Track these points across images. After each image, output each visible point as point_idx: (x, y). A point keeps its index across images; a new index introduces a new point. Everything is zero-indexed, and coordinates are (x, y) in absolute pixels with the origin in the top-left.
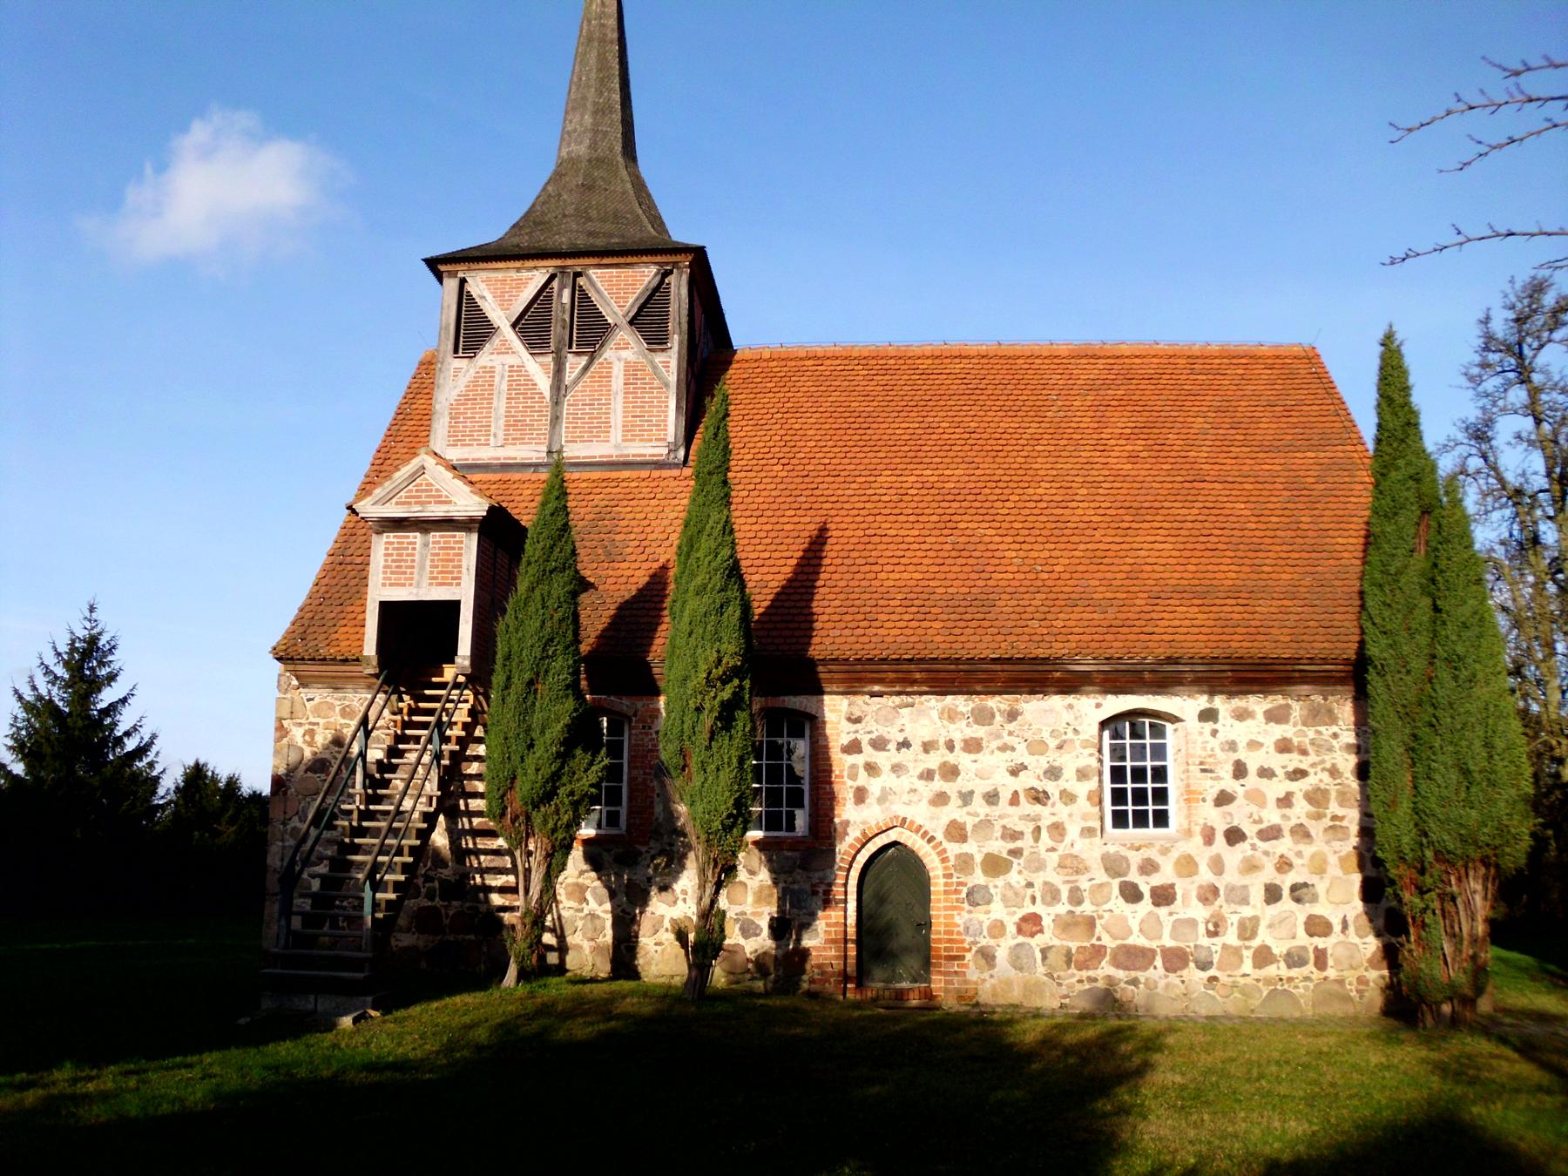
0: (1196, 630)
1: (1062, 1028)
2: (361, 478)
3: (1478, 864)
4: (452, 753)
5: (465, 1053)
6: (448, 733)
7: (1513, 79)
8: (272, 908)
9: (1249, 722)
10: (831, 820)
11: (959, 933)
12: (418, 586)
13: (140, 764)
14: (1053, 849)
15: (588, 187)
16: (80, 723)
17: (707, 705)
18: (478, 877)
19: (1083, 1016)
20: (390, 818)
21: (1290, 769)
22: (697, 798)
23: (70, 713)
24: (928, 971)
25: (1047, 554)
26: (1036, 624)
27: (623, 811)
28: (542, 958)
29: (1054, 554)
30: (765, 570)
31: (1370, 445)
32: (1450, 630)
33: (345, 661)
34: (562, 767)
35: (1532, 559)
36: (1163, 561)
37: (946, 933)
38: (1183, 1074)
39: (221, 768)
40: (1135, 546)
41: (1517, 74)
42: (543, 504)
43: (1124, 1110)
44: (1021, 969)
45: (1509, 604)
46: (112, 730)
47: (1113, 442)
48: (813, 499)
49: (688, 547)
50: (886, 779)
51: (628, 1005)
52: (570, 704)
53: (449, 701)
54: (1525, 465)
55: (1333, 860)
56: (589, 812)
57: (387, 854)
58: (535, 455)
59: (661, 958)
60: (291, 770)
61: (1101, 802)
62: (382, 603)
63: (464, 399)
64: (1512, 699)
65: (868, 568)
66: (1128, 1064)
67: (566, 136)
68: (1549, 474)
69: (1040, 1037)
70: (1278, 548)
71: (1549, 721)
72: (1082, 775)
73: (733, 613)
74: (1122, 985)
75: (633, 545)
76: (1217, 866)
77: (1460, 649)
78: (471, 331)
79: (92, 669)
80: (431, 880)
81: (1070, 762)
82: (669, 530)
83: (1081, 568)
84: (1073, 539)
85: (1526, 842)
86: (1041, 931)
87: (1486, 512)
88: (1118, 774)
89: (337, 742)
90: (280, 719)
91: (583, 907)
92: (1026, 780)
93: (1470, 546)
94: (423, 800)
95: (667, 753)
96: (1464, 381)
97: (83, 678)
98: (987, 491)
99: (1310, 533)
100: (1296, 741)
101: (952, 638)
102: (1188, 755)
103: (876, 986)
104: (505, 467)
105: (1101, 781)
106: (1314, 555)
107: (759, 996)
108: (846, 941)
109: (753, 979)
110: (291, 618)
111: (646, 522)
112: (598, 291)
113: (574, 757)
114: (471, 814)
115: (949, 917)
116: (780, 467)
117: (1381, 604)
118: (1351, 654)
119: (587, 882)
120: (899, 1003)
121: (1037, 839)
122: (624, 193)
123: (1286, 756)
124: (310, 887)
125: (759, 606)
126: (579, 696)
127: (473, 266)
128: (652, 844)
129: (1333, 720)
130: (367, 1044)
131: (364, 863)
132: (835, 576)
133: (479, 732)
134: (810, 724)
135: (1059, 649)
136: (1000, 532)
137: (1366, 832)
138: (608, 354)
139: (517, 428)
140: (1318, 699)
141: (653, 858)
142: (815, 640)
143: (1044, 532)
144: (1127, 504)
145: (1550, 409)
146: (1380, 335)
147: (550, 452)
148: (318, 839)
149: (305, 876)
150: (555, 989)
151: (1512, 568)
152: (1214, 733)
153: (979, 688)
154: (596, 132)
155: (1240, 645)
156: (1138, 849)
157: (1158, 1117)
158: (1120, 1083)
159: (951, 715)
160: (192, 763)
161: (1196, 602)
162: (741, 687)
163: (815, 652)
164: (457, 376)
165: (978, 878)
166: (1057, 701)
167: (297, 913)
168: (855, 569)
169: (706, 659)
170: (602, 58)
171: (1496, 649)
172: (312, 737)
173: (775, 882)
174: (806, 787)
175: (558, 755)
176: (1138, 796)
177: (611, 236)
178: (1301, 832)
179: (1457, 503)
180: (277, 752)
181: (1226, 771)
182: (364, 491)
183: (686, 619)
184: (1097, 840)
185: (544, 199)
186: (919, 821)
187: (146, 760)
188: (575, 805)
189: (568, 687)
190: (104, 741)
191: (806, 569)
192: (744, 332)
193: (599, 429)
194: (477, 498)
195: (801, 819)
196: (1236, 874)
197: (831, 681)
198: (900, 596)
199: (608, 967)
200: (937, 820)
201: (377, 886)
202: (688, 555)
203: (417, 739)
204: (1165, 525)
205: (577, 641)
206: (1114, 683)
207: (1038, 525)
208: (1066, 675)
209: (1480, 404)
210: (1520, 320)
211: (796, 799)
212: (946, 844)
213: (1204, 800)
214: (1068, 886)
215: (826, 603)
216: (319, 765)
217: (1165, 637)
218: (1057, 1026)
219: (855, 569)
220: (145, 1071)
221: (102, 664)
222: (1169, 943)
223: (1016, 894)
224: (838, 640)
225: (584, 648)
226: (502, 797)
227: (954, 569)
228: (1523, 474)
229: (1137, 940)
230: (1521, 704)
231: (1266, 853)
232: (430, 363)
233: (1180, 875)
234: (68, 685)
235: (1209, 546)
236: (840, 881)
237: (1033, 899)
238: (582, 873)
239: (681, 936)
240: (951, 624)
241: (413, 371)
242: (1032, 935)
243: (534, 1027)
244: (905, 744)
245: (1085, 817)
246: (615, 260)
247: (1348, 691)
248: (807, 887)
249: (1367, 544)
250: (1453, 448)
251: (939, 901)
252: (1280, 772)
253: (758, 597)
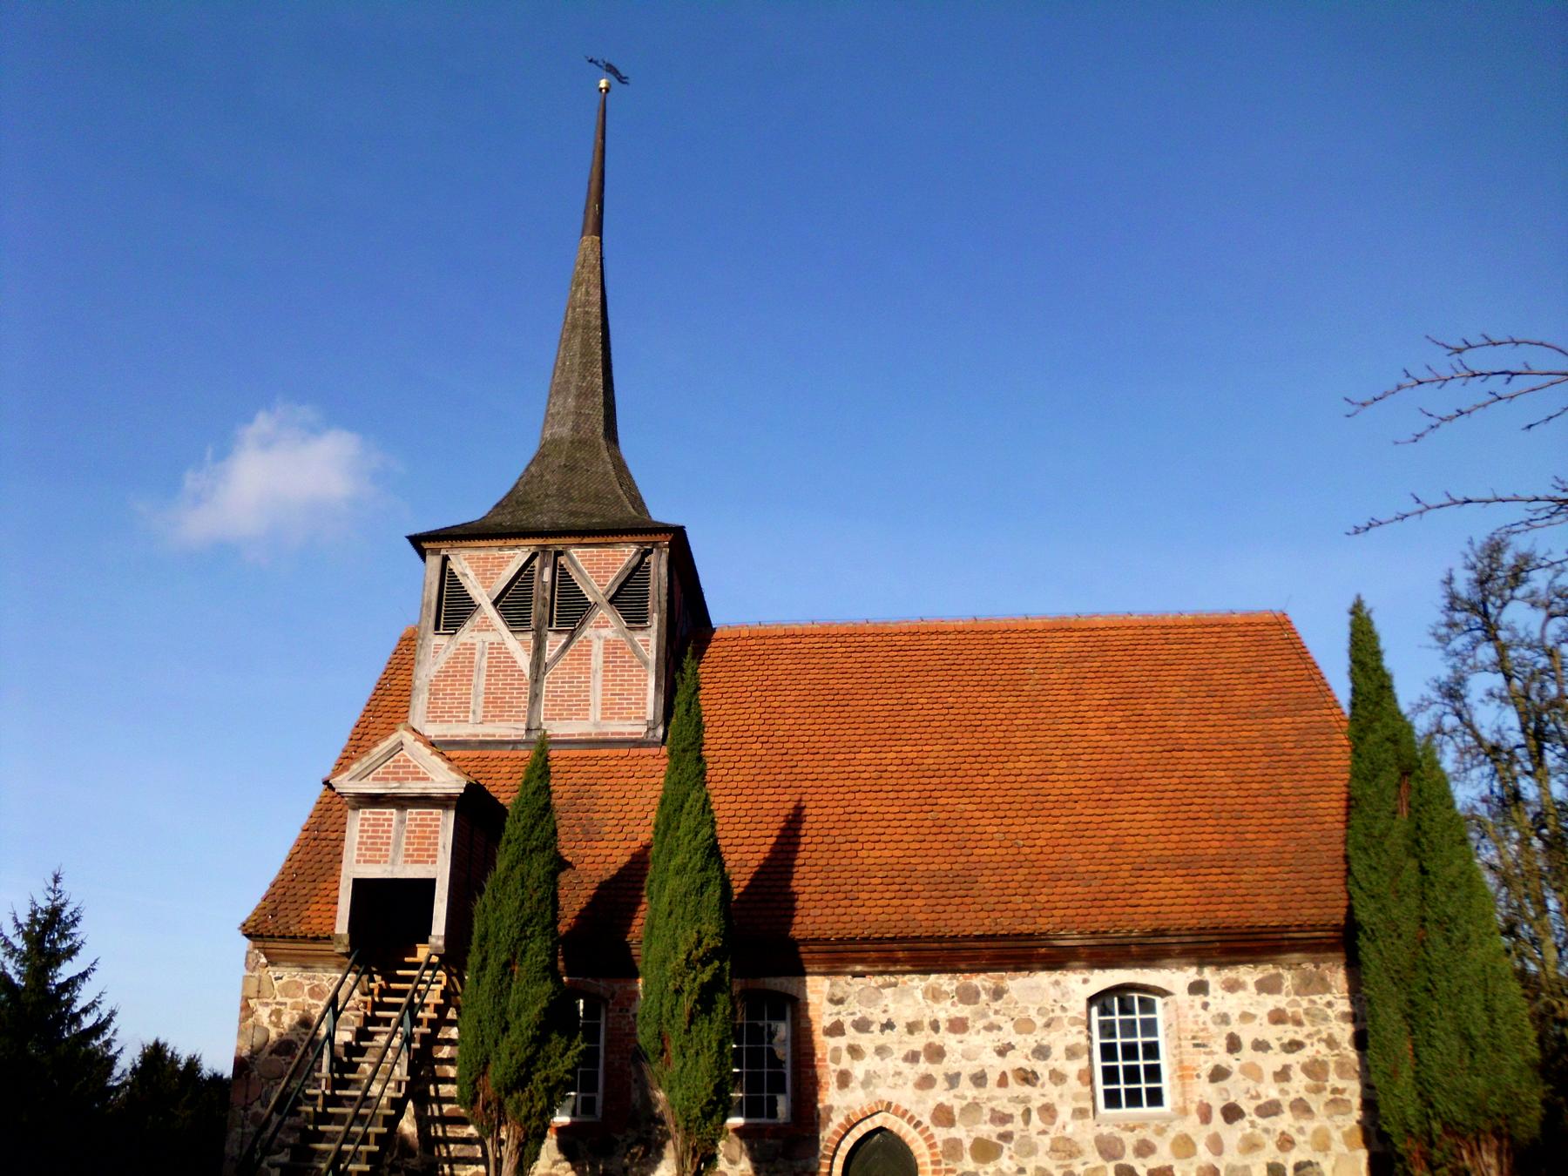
0: (1182, 901)
2: (339, 753)
3: (1490, 1136)
4: (423, 1035)
6: (420, 1014)
7: (1457, 356)
9: (1241, 993)
10: (814, 1106)
12: (393, 863)
13: (96, 1043)
14: (1044, 1132)
15: (571, 467)
17: (687, 988)
20: (356, 1104)
21: (1286, 1040)
22: (676, 1084)
26: (1019, 899)
27: (599, 1098)
30: (744, 849)
31: (1346, 709)
32: (1438, 892)
33: (316, 939)
34: (537, 1052)
35: (1515, 815)
39: (182, 1047)
40: (1117, 817)
41: (1459, 351)
42: (526, 783)
45: (1496, 862)
47: (1091, 714)
48: (792, 777)
49: (666, 826)
50: (870, 1062)
52: (548, 986)
54: (1499, 721)
55: (1337, 1136)
56: (564, 1098)
57: (351, 1142)
58: (513, 732)
60: (255, 1052)
61: (1092, 1081)
62: (355, 881)
63: (445, 674)
64: (1507, 960)
65: (848, 846)
67: (549, 418)
68: (1524, 730)
70: (1260, 815)
71: (1548, 981)
72: (1072, 1053)
73: (713, 893)
75: (611, 828)
76: (1216, 1145)
77: (1450, 910)
78: (453, 608)
79: (53, 942)
81: (1060, 1040)
82: (648, 808)
84: (1054, 812)
85: (1537, 1112)
87: (1466, 770)
88: (1108, 1052)
89: (305, 1022)
90: (246, 999)
92: (1016, 1060)
93: (1452, 805)
94: (392, 1085)
95: (645, 1036)
96: (1432, 641)
99: (1291, 799)
100: (1289, 1011)
101: (933, 916)
102: (1179, 1030)
104: (483, 744)
105: (1091, 1059)
106: (1296, 820)
110: (262, 893)
111: (624, 801)
112: (579, 570)
113: (550, 1041)
114: (441, 1100)
116: (759, 745)
117: (1363, 865)
118: (1340, 919)
121: (1027, 1121)
123: (1280, 1027)
125: (739, 885)
126: (556, 978)
127: (458, 544)
129: (1326, 988)
131: (327, 1152)
132: (815, 855)
133: (451, 1014)
134: (794, 1007)
135: (1043, 924)
136: (982, 807)
137: (1369, 1105)
138: (588, 632)
139: (496, 705)
140: (1310, 967)
141: (630, 1147)
142: (797, 920)
144: (1107, 776)
145: (1519, 665)
146: (1349, 605)
147: (528, 730)
148: (280, 1124)
149: (264, 1165)
151: (1495, 825)
152: (1205, 1006)
153: (963, 966)
154: (579, 414)
155: (1225, 914)
159: (935, 995)
161: (1180, 872)
162: (721, 969)
163: (797, 932)
164: (438, 652)
166: (1043, 978)
168: (835, 847)
170: (585, 344)
171: (1487, 909)
172: (279, 1019)
174: (788, 1071)
175: (534, 1039)
176: (1130, 1075)
177: (592, 516)
178: (1302, 1108)
179: (1435, 764)
180: (241, 1033)
181: (1219, 1045)
182: (342, 766)
183: (666, 899)
184: (1089, 1121)
185: (528, 478)
186: (905, 1105)
187: (103, 1039)
188: (550, 1092)
189: (545, 969)
190: (60, 1018)
192: (723, 610)
194: (455, 776)
195: (783, 1105)
196: (1236, 1153)
198: (881, 874)
202: (665, 834)
203: (387, 1021)
204: (1146, 795)
205: (555, 921)
206: (1101, 957)
207: (1018, 799)
208: (1053, 951)
209: (1450, 663)
210: (1482, 582)
212: (933, 1129)
213: (1198, 1076)
214: (1062, 1171)
215: (806, 882)
216: (285, 1047)
217: (1152, 909)
219: (835, 847)
221: (63, 936)
225: (562, 928)
226: (474, 1083)
227: (936, 845)
228: (1499, 730)
230: (1518, 965)
231: (1266, 1131)
232: (411, 639)
233: (1178, 1156)
234: (24, 958)
235: (1191, 815)
238: (555, 1163)
244: (889, 1025)
245: (1076, 1097)
247: (1339, 958)
249: (1348, 807)
250: (1427, 708)
252: (1275, 1044)
253: (738, 877)
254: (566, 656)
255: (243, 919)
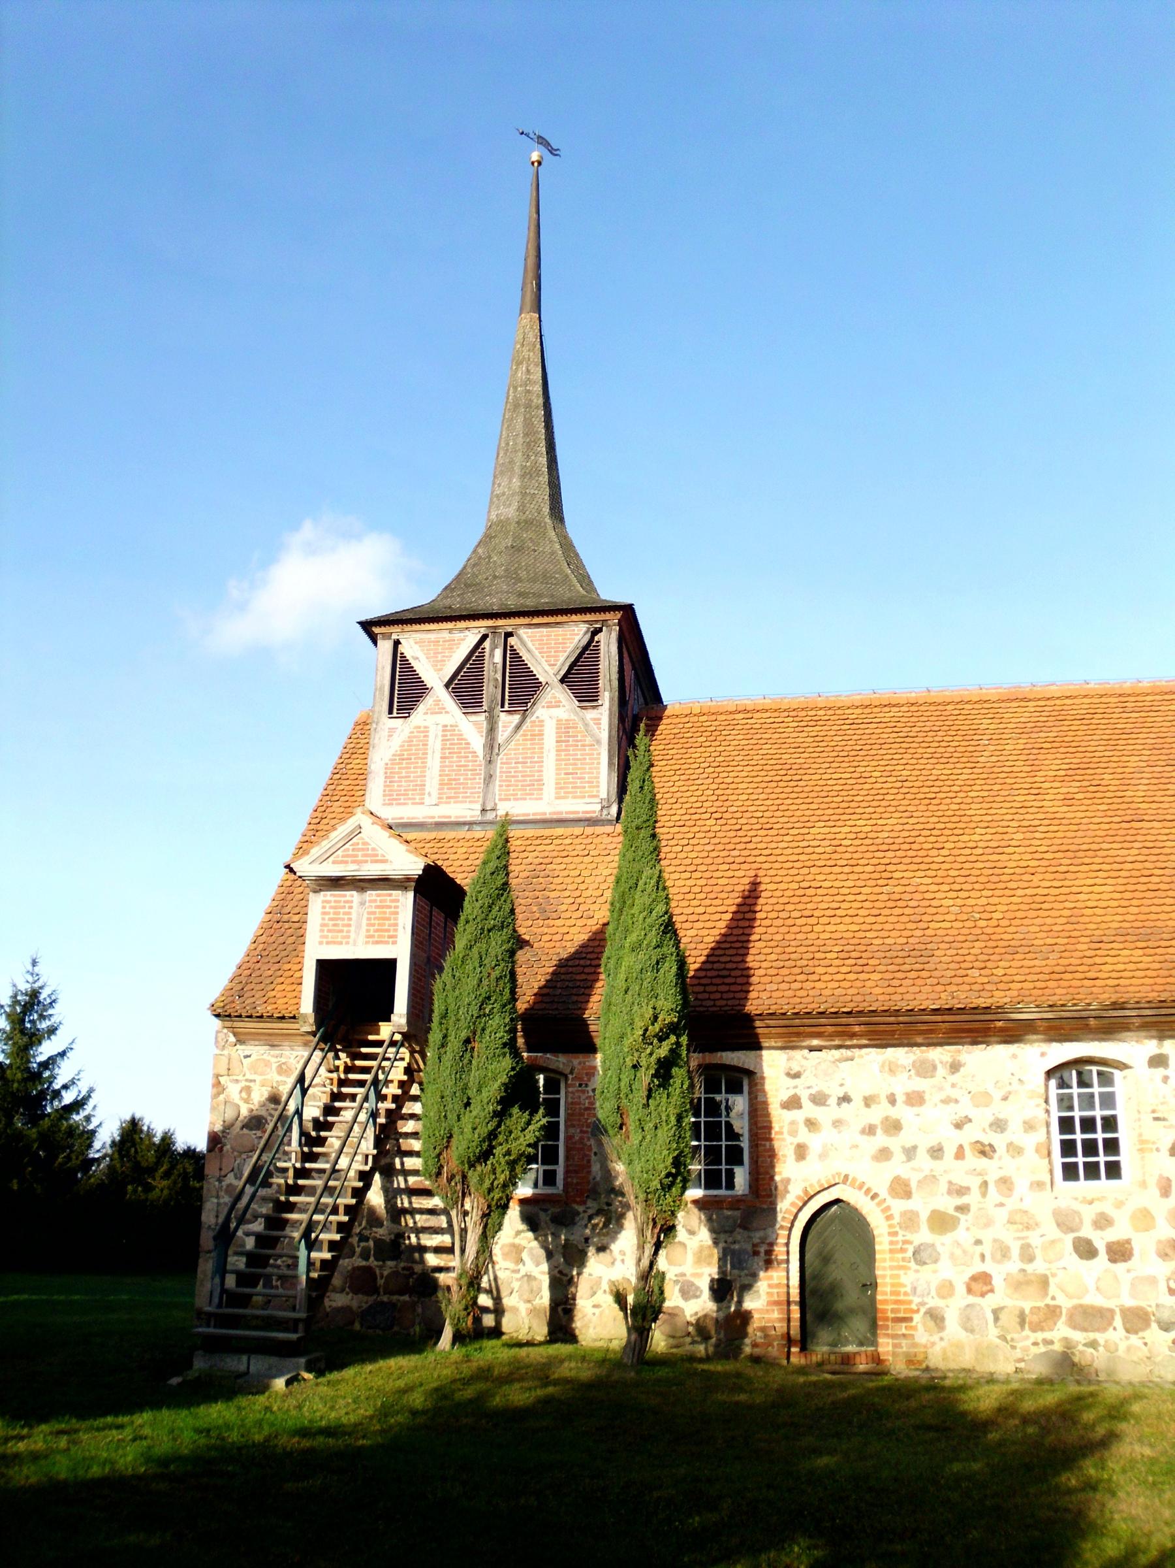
1: (1018, 1394)
4: (388, 1111)
5: (400, 1418)
8: (206, 1266)
10: (772, 1178)
11: (906, 1294)
14: (1002, 1205)
15: (517, 549)
16: (19, 1075)
17: (643, 1063)
18: (413, 1236)
19: (1040, 1382)
22: (635, 1157)
23: (10, 1066)
24: (875, 1334)
25: (984, 901)
26: (976, 973)
27: (560, 1169)
28: (477, 1320)
29: (991, 900)
30: (699, 925)
34: (499, 1126)
36: (1104, 904)
37: (892, 1293)
38: (1151, 1446)
39: (157, 1123)
40: (1074, 890)
43: (1091, 1486)
44: (972, 1331)
46: (51, 1083)
49: (620, 904)
51: (567, 1370)
52: (507, 1062)
53: (385, 1059)
56: (525, 1171)
57: (322, 1212)
59: (600, 1323)
60: (228, 1127)
61: (1049, 1154)
62: (318, 961)
66: (1091, 1436)
67: (495, 498)
69: (996, 1405)
72: (1029, 1126)
73: (669, 969)
74: (1080, 1347)
78: (406, 691)
79: (33, 1022)
80: (367, 1239)
82: (603, 886)
83: (1019, 914)
86: (992, 1291)
88: (1066, 1125)
89: (274, 1099)
90: (217, 1076)
91: (519, 1269)
94: (359, 1158)
95: (604, 1111)
97: (23, 1031)
98: (921, 839)
101: (891, 990)
103: (821, 1350)
104: (439, 825)
105: (1048, 1132)
107: (701, 1360)
108: (789, 1303)
109: (693, 1342)
110: (230, 975)
111: (580, 880)
113: (511, 1116)
114: (406, 1173)
115: (896, 1278)
116: (713, 822)
119: (524, 1243)
120: (845, 1368)
121: (984, 1194)
122: (553, 553)
124: (244, 1245)
125: (694, 963)
126: (516, 1053)
127: (408, 628)
128: (590, 1203)
130: (299, 1407)
132: (770, 930)
133: (415, 1090)
134: (743, 1079)
135: (999, 998)
141: (590, 1218)
142: (752, 995)
143: (981, 879)
144: (1064, 848)
147: (484, 810)
149: (240, 1233)
150: (490, 1353)
153: (919, 1040)
156: (1091, 1203)
157: (1128, 1494)
158: (1084, 1456)
159: (892, 1069)
160: (128, 1118)
162: (678, 1044)
163: (752, 1007)
164: (391, 736)
165: (923, 1235)
167: (232, 1272)
168: (790, 922)
169: (642, 1016)
170: (528, 423)
172: (249, 1094)
173: (716, 1243)
174: (745, 1144)
175: (496, 1114)
176: (1089, 1148)
177: (541, 596)
180: (213, 1109)
183: (622, 976)
185: (475, 561)
187: (83, 1114)
188: (512, 1164)
189: (505, 1045)
190: (42, 1095)
191: (741, 924)
193: (534, 786)
195: (741, 1177)
197: (769, 1036)
198: (837, 949)
199: (545, 1330)
200: (879, 1177)
201: (311, 1245)
203: (353, 1097)
205: (513, 998)
206: (1061, 1028)
207: (974, 872)
208: (1010, 1025)
211: (735, 1157)
212: (890, 1201)
213: (1158, 1150)
215: (762, 957)
216: (255, 1122)
218: (1013, 1392)
219: (790, 922)
220: (76, 1431)
221: (42, 1017)
222: (1130, 1303)
223: (965, 1252)
224: (775, 994)
225: (521, 1006)
229: (1094, 1299)
232: (365, 723)
233: (1137, 1230)
236: (782, 1240)
237: (983, 1257)
238: (518, 1233)
239: (620, 1299)
240: (888, 976)
241: (348, 731)
242: (983, 1295)
243: (469, 1393)
244: (846, 1099)
246: (545, 620)
248: (749, 1247)
251: (884, 1260)
253: (694, 953)
254: (518, 736)
255: (212, 1001)
